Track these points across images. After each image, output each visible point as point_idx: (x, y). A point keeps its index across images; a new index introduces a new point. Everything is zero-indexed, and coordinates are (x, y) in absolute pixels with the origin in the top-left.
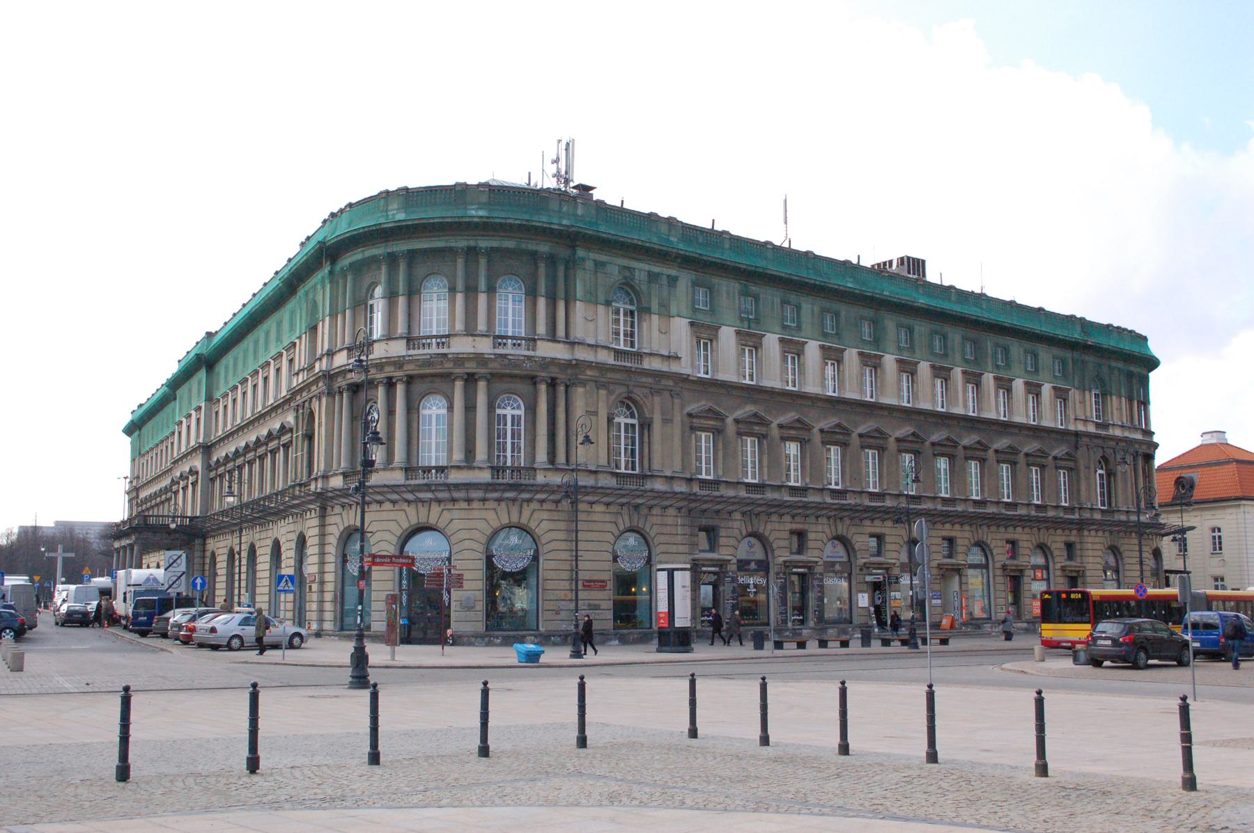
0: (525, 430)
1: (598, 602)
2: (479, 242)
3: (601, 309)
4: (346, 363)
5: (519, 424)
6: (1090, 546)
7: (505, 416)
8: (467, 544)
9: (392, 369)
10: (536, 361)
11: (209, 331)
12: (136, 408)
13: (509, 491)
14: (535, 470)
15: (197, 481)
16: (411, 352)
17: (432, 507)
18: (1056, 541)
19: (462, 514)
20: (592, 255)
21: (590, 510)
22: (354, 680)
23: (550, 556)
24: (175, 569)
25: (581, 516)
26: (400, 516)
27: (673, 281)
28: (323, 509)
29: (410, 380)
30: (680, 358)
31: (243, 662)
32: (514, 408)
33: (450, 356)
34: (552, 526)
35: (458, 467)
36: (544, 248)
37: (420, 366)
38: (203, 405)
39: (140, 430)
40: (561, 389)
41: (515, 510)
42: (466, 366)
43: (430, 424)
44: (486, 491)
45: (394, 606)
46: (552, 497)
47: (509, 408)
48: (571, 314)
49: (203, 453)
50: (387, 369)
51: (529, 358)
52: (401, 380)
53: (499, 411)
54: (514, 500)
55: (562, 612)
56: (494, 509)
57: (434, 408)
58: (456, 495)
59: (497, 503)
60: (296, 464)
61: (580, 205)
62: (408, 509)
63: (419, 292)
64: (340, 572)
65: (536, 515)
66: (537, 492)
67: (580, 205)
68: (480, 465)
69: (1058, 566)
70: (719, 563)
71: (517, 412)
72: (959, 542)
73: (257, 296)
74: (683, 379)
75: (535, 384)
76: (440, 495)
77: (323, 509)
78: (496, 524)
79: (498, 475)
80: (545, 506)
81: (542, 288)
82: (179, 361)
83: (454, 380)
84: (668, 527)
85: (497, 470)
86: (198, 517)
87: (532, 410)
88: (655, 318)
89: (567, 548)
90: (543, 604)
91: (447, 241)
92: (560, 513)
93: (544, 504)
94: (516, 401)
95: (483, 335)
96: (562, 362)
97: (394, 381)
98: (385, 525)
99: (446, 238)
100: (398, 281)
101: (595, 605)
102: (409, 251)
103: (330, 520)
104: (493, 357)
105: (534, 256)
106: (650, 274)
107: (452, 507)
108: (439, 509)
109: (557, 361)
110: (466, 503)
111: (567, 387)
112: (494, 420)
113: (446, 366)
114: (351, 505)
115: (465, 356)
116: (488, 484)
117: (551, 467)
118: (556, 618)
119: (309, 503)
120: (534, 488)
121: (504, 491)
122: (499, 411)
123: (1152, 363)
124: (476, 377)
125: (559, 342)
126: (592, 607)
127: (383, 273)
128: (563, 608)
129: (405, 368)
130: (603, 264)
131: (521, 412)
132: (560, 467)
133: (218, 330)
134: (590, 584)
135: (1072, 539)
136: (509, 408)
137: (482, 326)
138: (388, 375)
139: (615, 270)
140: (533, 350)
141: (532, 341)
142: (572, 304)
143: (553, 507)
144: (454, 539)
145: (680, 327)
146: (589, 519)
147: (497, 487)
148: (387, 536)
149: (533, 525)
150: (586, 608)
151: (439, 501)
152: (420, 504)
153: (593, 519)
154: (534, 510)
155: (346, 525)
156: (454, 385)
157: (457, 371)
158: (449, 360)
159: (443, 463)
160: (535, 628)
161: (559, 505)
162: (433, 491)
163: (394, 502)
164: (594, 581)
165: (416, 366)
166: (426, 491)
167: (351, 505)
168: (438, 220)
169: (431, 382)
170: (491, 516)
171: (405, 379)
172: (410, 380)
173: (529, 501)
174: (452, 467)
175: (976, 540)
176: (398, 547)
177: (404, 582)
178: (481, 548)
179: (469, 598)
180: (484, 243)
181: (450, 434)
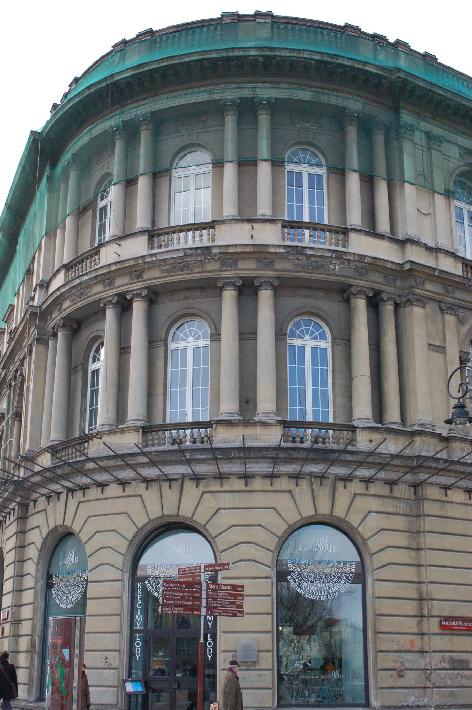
0: (333, 370)
2: (258, 90)
3: (440, 200)
5: (324, 363)
9: (126, 280)
10: (349, 260)
13: (313, 461)
14: (353, 429)
19: (237, 500)
20: (423, 125)
21: (444, 498)
22: (294, 595)
23: (383, 574)
32: (315, 338)
33: (214, 251)
34: (385, 522)
35: (229, 423)
37: (168, 271)
40: (389, 308)
42: (240, 266)
43: (184, 384)
44: (276, 460)
45: (66, 652)
46: (382, 475)
47: (307, 337)
48: (398, 204)
50: (119, 282)
51: (339, 255)
52: (139, 295)
53: (291, 341)
54: (322, 477)
55: (408, 673)
56: (290, 492)
58: (226, 468)
61: (402, 55)
62: (146, 494)
63: (168, 171)
64: (41, 604)
65: (359, 502)
66: (360, 464)
67: (402, 55)
68: (265, 420)
71: (319, 344)
75: (347, 301)
76: (200, 469)
80: (373, 489)
83: (221, 289)
84: (135, 699)
89: (412, 562)
90: (375, 658)
91: (209, 92)
92: (396, 503)
93: (371, 485)
94: (318, 327)
95: (265, 221)
96: (389, 266)
98: (108, 523)
99: (208, 88)
100: (138, 157)
102: (153, 114)
103: (33, 521)
104: (282, 250)
107: (217, 488)
109: (381, 263)
110: (242, 481)
111: (397, 306)
114: (59, 494)
115: (239, 250)
116: (279, 449)
117: (380, 425)
118: (399, 684)
120: (354, 458)
121: (305, 461)
122: (291, 341)
125: (381, 237)
126: (457, 664)
127: (116, 160)
128: (408, 665)
129: (145, 277)
130: (440, 140)
131: (327, 344)
132: (392, 426)
136: (307, 337)
139: (455, 152)
140: (344, 247)
142: (398, 187)
143: (384, 490)
144: (221, 543)
146: (443, 513)
147: (295, 455)
149: (354, 520)
150: (446, 665)
152: (165, 485)
153: (450, 514)
155: (52, 526)
156: (221, 296)
158: (213, 259)
159: (205, 417)
160: (363, 701)
161: (396, 488)
162: (188, 462)
163: (124, 483)
164: (456, 619)
165: (163, 271)
166: (177, 462)
167: (59, 494)
168: (196, 58)
169: (187, 298)
173: (346, 479)
174: (220, 422)
176: (129, 559)
177: (139, 618)
178: (268, 558)
179: (247, 648)
181: (216, 377)
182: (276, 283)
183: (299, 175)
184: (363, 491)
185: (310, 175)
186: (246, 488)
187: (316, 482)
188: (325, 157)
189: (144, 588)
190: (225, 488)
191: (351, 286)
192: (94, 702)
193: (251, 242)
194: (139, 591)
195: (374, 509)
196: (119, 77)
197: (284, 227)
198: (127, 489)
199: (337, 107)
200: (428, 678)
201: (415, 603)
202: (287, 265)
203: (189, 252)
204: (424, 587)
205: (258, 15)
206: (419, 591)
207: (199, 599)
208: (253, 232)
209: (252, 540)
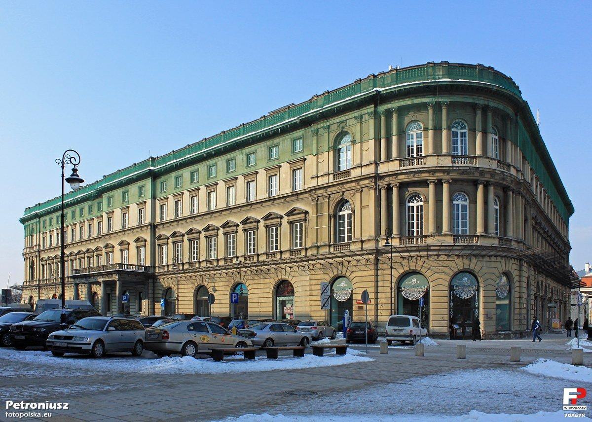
6: (250, 287)
7: (413, 207)
16: (402, 168)
19: (488, 264)
26: (452, 264)
28: (39, 289)
29: (403, 186)
31: (415, 373)
41: (467, 262)
42: (486, 176)
71: (464, 203)
77: (39, 289)
79: (409, 242)
85: (456, 237)
87: (474, 201)
97: (391, 186)
105: (474, 107)
107: (482, 260)
112: (452, 207)
113: (476, 175)
131: (467, 203)
141: (377, 163)
151: (475, 256)
157: (481, 179)
169: (462, 184)
170: (498, 265)
171: (398, 185)
175: (504, 269)
180: (492, 104)
182: (485, 183)
186: (496, 260)
189: (453, 293)
190: (484, 260)
192: (289, 246)
193: (488, 167)
194: (452, 295)
203: (471, 168)
205: (490, 68)
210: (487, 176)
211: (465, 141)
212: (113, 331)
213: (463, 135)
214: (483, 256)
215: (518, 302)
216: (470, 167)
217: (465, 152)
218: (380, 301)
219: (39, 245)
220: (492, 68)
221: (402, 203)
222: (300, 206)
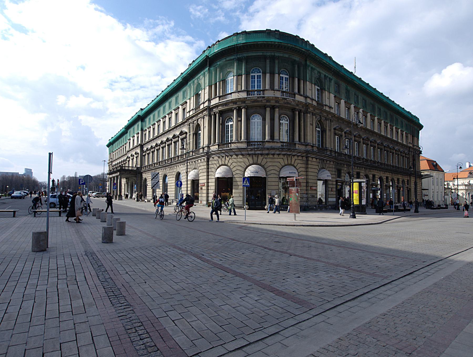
1: (314, 195)
3: (313, 85)
4: (218, 102)
8: (272, 172)
9: (241, 103)
11: (142, 108)
12: (110, 139)
15: (138, 156)
17: (259, 157)
18: (406, 179)
20: (318, 69)
24: (155, 181)
25: (309, 162)
27: (330, 80)
29: (221, 113)
30: (333, 108)
32: (285, 121)
36: (297, 58)
38: (140, 132)
39: (112, 145)
42: (271, 102)
49: (140, 147)
56: (283, 158)
57: (256, 119)
59: (283, 156)
60: (144, 161)
69: (384, 185)
70: (341, 182)
72: (376, 176)
73: (164, 92)
74: (333, 115)
78: (283, 164)
81: (268, 69)
82: (128, 121)
86: (139, 167)
87: (264, 119)
88: (326, 92)
95: (277, 90)
101: (313, 196)
105: (265, 58)
106: (325, 75)
107: (267, 157)
108: (262, 158)
119: (177, 164)
123: (421, 127)
124: (275, 107)
125: (301, 95)
128: (304, 197)
133: (145, 108)
134: (332, 189)
135: (409, 179)
137: (276, 87)
138: (239, 105)
141: (209, 100)
145: (332, 96)
146: (312, 164)
148: (240, 168)
150: (311, 197)
151: (262, 155)
152: (254, 156)
154: (296, 159)
157: (268, 104)
170: (281, 161)
172: (247, 108)
183: (283, 77)
184: (297, 158)
185: (285, 78)
186: (273, 157)
187: (288, 156)
188: (289, 73)
190: (268, 157)
191: (295, 108)
193: (274, 96)
195: (299, 163)
196: (239, 45)
197: (281, 92)
198: (244, 156)
199: (293, 59)
200: (307, 199)
201: (305, 183)
202: (282, 102)
204: (308, 180)
206: (307, 181)
207: (295, 184)
208: (274, 93)
209: (274, 169)
210: (272, 102)
211: (260, 80)
212: (348, 218)
213: (259, 77)
214: (268, 154)
215: (305, 185)
216: (258, 97)
217: (260, 87)
218: (210, 184)
219: (112, 158)
220: (278, 31)
221: (223, 124)
222: (185, 129)
